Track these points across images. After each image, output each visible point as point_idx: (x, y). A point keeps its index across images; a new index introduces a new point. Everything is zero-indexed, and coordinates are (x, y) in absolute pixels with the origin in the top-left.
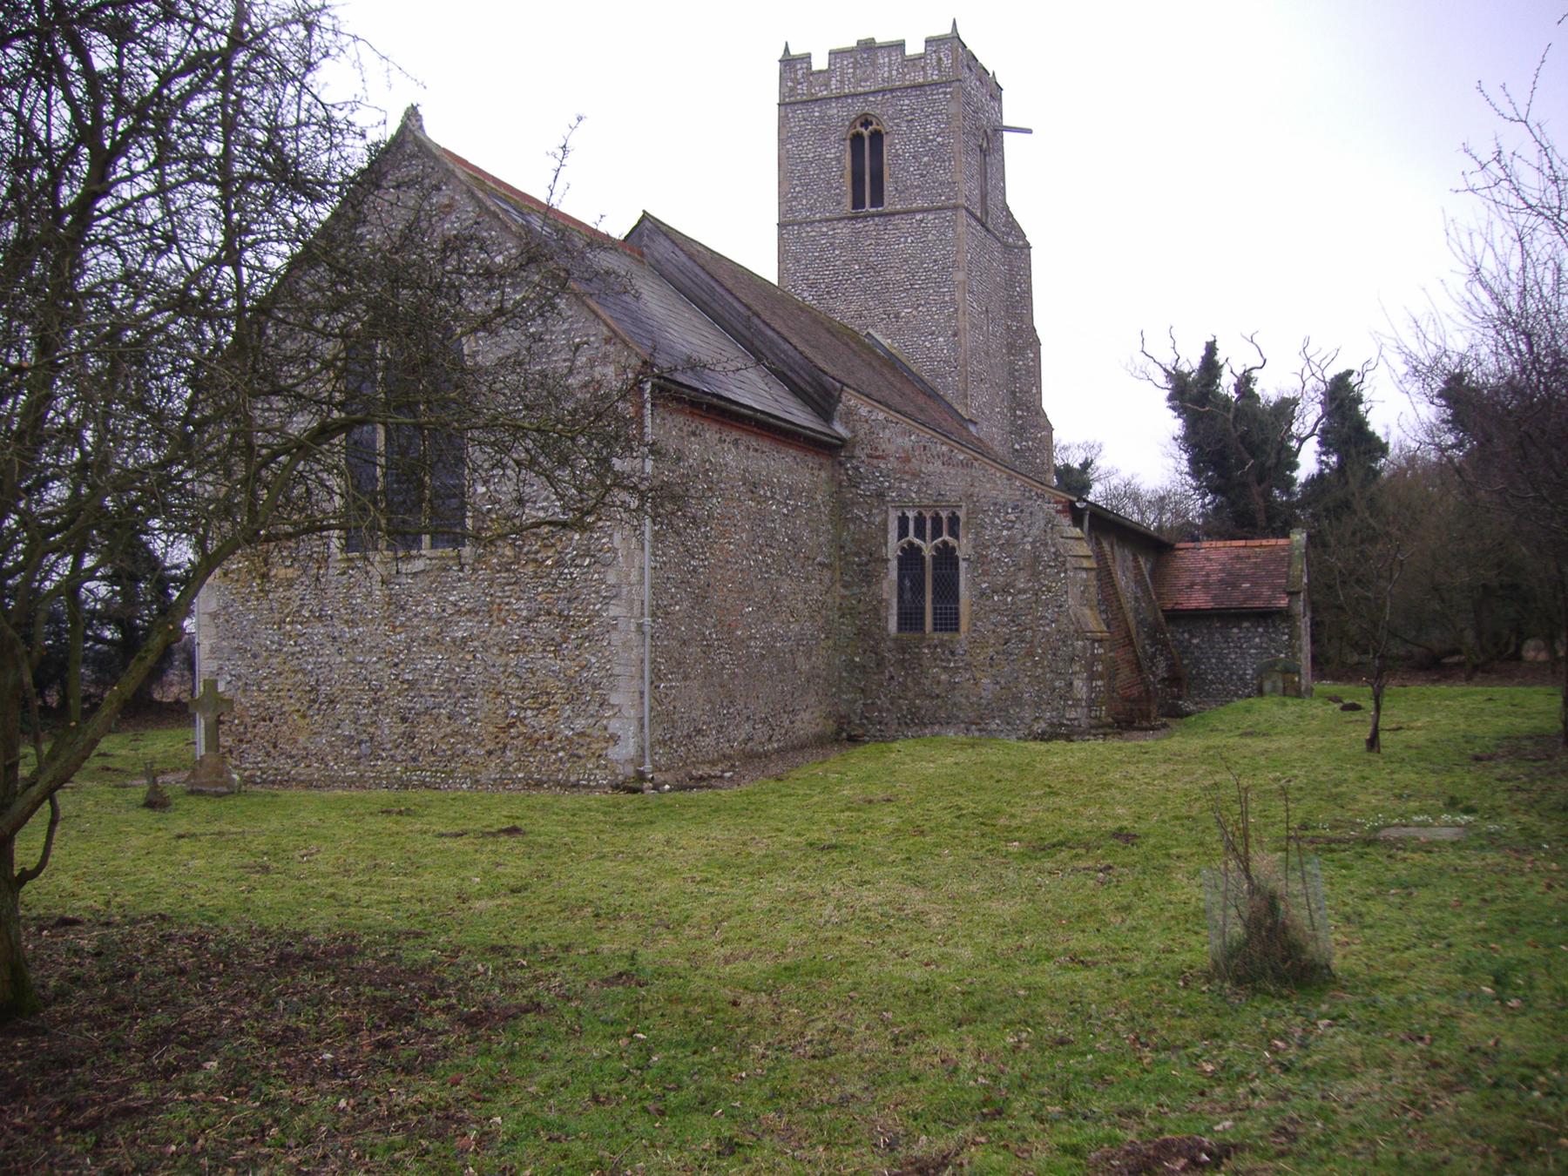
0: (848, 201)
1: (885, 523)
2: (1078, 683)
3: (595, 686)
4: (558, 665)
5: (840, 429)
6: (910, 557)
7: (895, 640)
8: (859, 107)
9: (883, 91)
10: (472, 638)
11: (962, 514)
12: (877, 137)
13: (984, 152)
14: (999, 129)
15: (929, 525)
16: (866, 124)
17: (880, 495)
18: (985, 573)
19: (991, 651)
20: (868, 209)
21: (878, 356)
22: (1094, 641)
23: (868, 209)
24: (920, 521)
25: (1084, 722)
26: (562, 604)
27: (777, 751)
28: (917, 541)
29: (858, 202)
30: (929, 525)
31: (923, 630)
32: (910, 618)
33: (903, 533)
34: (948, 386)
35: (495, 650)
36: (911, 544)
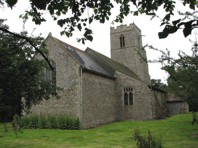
0: (120, 46)
1: (122, 89)
2: (151, 112)
3: (74, 114)
4: (69, 111)
5: (115, 76)
6: (126, 94)
7: (124, 106)
8: (121, 34)
9: (124, 31)
10: (57, 107)
11: (133, 88)
12: (124, 37)
13: (139, 39)
14: (141, 36)
15: (126, 89)
16: (122, 36)
17: (121, 85)
18: (137, 96)
19: (138, 108)
20: (123, 47)
21: (124, 67)
22: (153, 106)
23: (123, 47)
24: (127, 89)
25: (152, 118)
26: (69, 102)
27: (105, 123)
28: (127, 92)
29: (121, 46)
30: (126, 89)
31: (128, 105)
32: (126, 103)
33: (125, 91)
34: (134, 71)
35: (60, 109)
36: (126, 92)
